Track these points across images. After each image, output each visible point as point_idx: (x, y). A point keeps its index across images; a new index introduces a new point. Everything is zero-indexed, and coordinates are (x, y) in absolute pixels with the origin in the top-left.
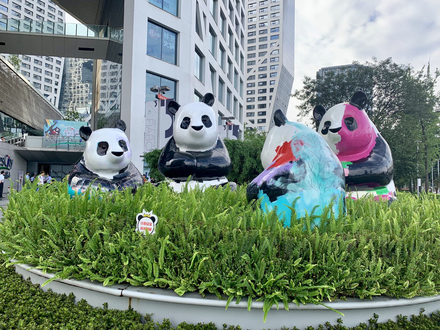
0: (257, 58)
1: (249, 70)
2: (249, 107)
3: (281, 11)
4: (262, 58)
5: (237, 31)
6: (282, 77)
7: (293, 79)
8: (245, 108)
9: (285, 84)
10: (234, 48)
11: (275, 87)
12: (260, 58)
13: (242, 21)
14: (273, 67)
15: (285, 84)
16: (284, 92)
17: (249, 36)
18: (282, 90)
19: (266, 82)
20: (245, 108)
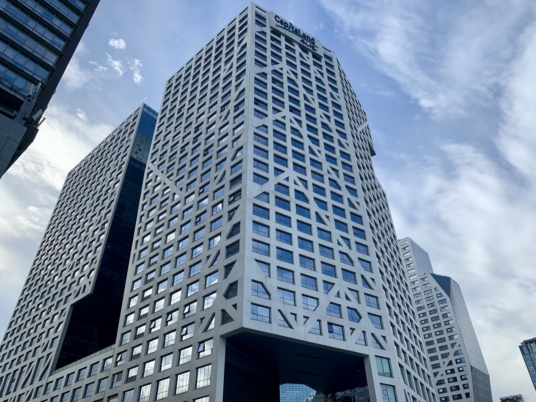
0: (440, 361)
1: (435, 374)
2: (428, 343)
3: (451, 311)
4: (447, 361)
5: (405, 296)
6: (474, 378)
7: (488, 377)
8: (428, 360)
9: (480, 385)
10: (412, 349)
11: (470, 390)
12: (444, 360)
13: (411, 303)
14: (447, 323)
15: (480, 385)
16: (483, 395)
17: (418, 310)
18: (480, 393)
19: (459, 389)
20: (428, 360)
